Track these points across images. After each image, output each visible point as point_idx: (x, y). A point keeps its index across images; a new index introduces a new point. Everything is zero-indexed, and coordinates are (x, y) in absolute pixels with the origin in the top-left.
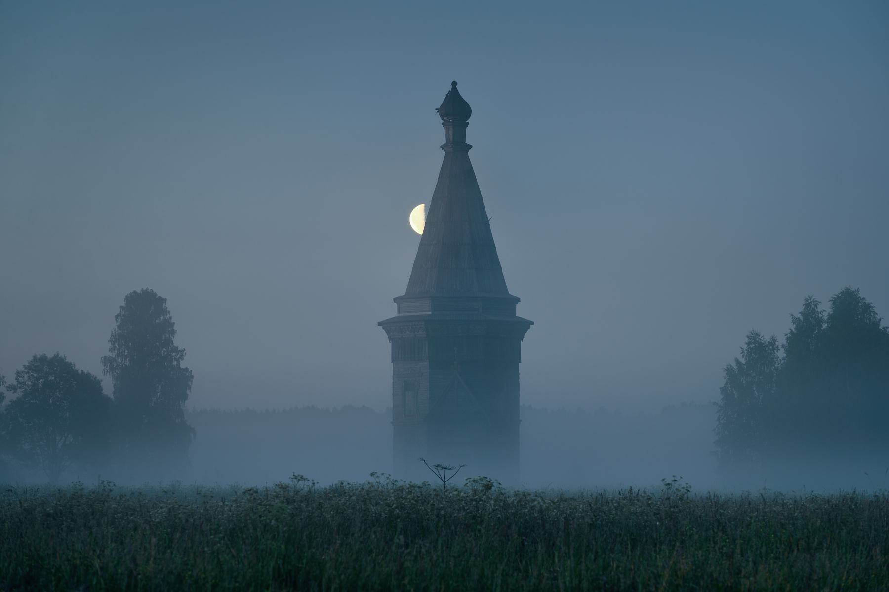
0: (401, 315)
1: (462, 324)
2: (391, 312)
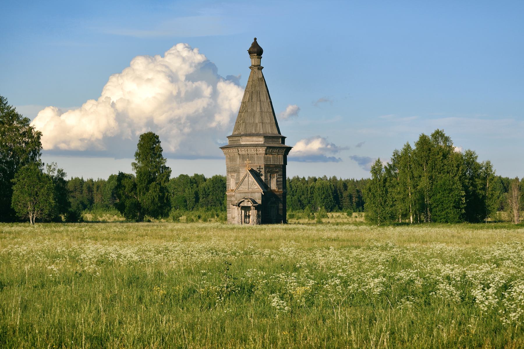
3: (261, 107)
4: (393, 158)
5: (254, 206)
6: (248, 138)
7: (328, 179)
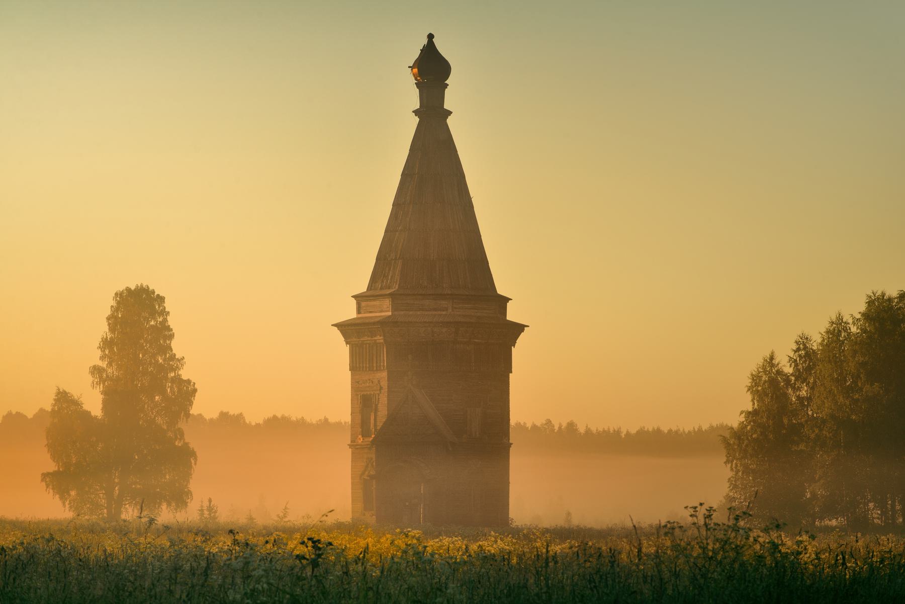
0: (360, 316)
1: (437, 308)
2: (350, 312)
4: (795, 356)
7: (556, 428)
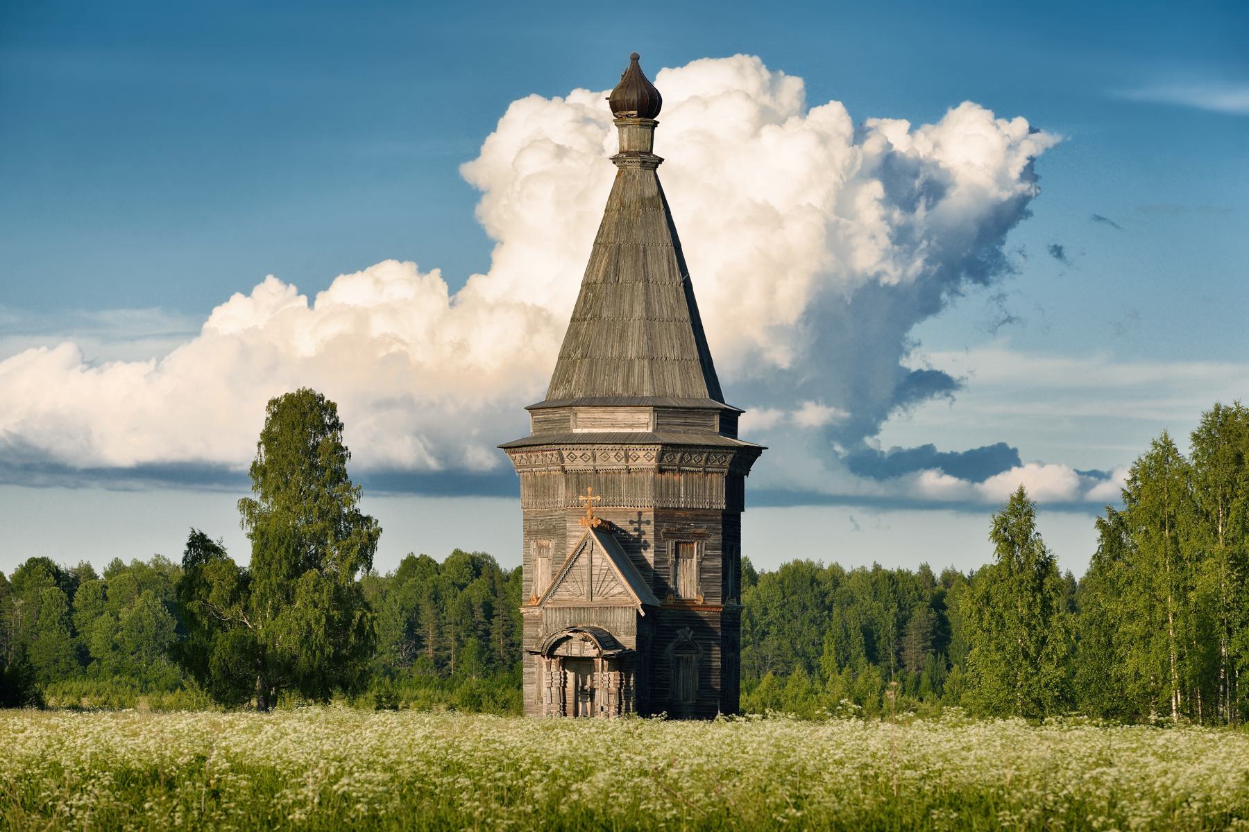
3: (648, 304)
5: (605, 658)
6: (598, 413)
